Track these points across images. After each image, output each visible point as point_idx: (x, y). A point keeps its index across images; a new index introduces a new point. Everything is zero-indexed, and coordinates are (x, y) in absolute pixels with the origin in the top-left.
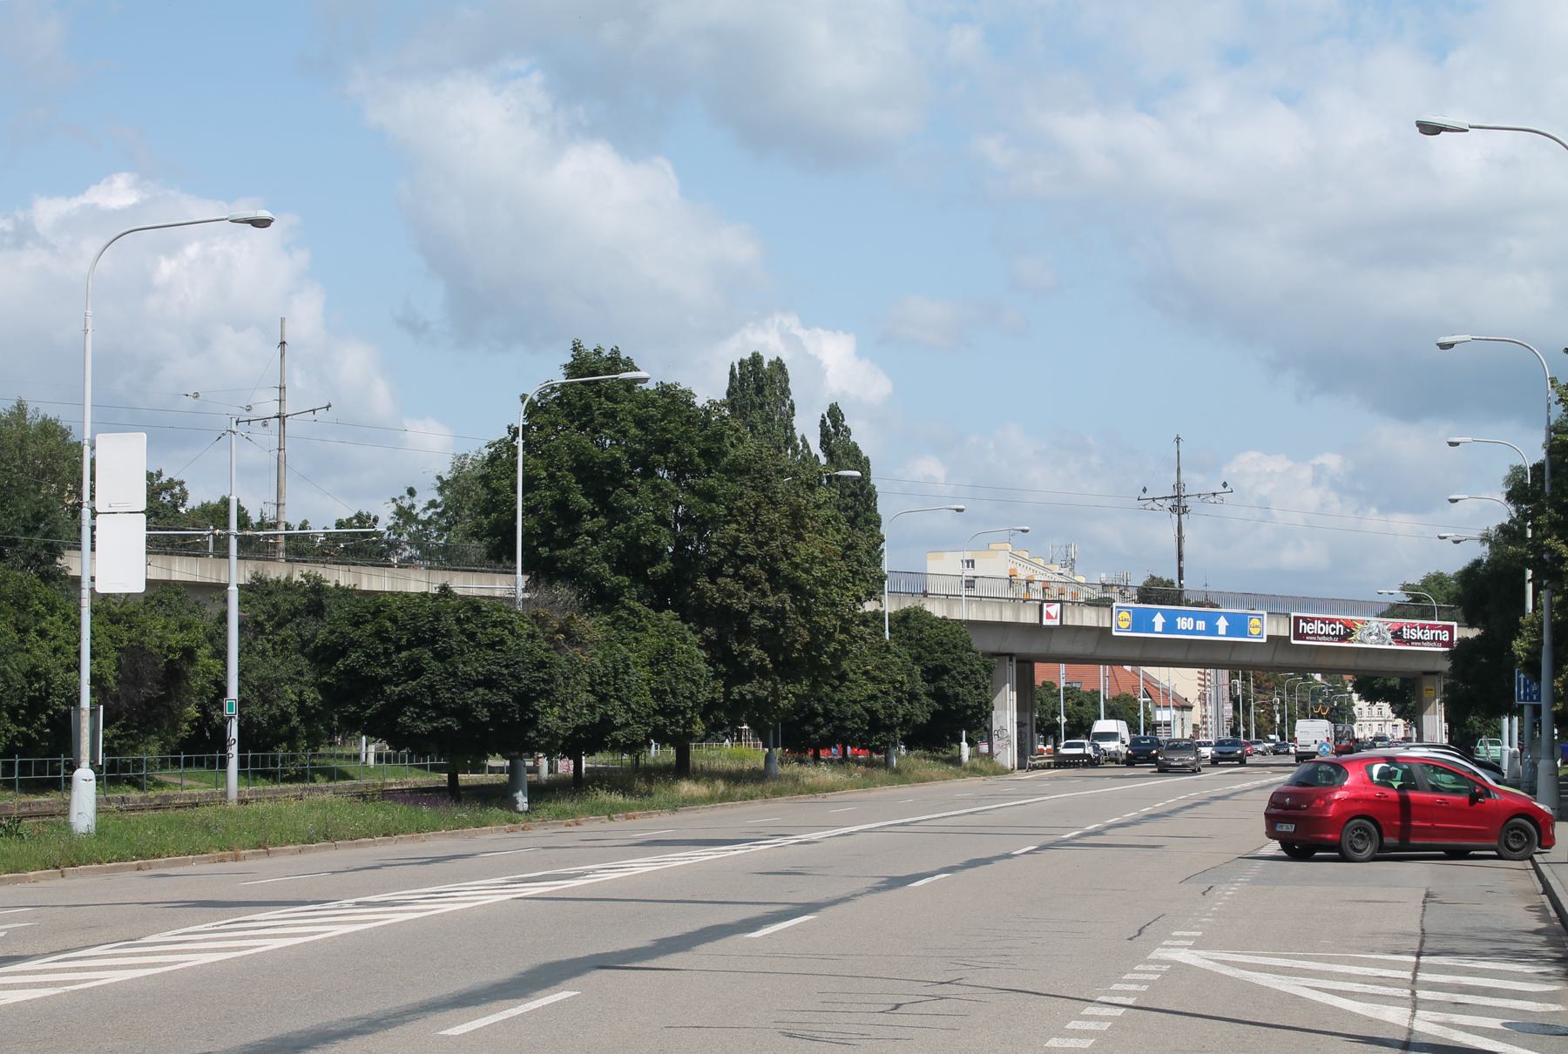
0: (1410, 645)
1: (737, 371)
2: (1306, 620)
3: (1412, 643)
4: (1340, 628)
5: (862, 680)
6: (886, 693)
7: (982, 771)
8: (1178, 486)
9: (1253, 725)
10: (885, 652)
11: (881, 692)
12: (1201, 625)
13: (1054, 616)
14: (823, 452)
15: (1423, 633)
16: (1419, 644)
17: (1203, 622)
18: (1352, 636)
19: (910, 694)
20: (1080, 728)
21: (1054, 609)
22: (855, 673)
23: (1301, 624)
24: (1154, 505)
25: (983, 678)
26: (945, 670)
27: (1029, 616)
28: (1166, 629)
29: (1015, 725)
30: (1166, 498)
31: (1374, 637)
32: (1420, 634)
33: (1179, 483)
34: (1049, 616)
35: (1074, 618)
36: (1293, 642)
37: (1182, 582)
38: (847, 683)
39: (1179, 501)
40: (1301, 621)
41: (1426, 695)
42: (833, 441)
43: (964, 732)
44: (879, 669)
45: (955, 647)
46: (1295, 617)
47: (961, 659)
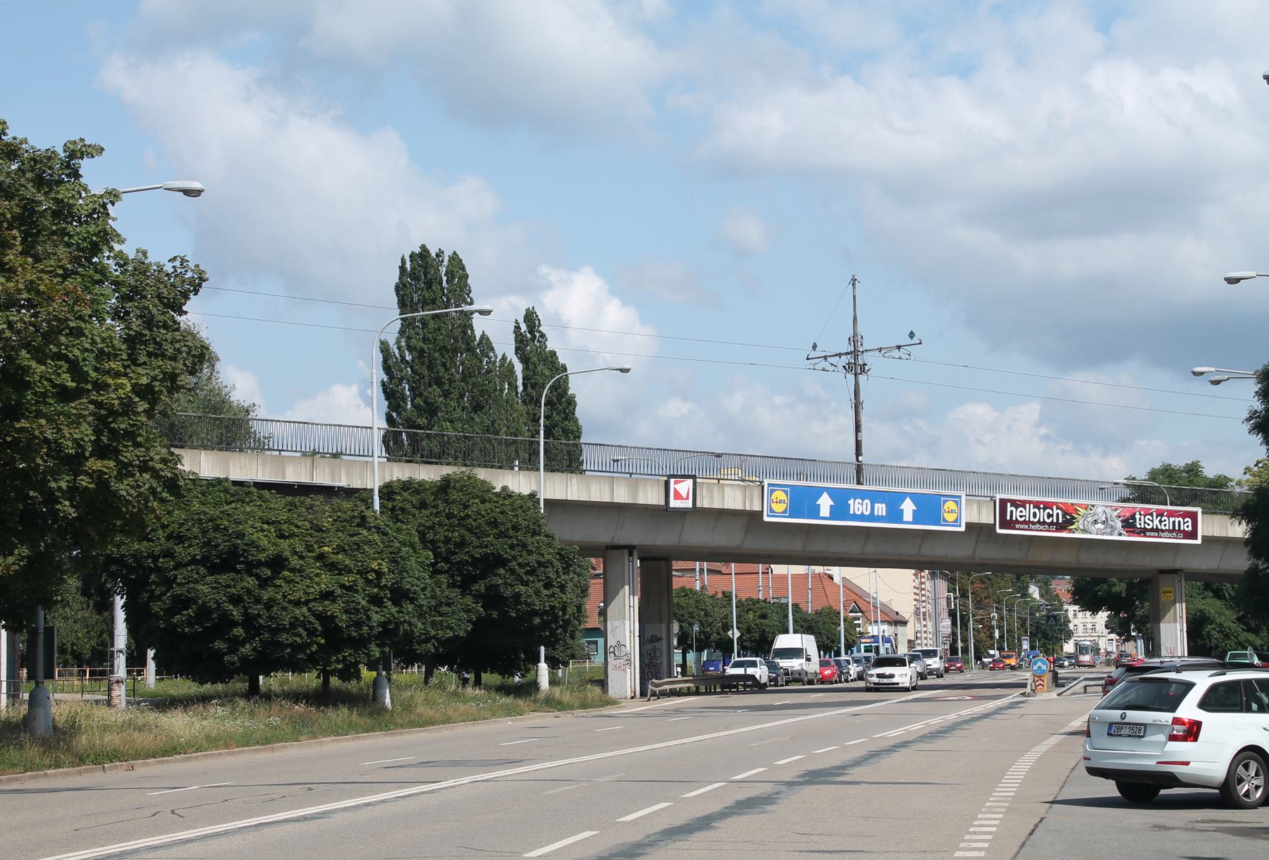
0: (1145, 536)
1: (408, 265)
2: (1015, 504)
3: (1148, 534)
4: (1058, 514)
5: (314, 568)
6: (350, 589)
7: (560, 703)
8: (855, 339)
9: (972, 641)
10: (358, 525)
11: (342, 586)
12: (881, 509)
13: (685, 496)
14: (519, 358)
15: (1161, 522)
16: (1156, 534)
17: (884, 505)
18: (1073, 524)
19: (392, 590)
20: (760, 645)
21: (685, 487)
22: (301, 557)
23: (1009, 508)
24: (824, 364)
25: (557, 572)
26: (500, 561)
27: (651, 496)
28: (834, 514)
29: (637, 639)
30: (840, 355)
31: (1100, 526)
32: (1156, 522)
33: (855, 335)
34: (678, 496)
35: (712, 497)
36: (999, 531)
37: (860, 458)
38: (286, 573)
39: (856, 357)
40: (1009, 504)
41: (1164, 598)
42: (529, 348)
43: (542, 648)
44: (344, 550)
45: (515, 528)
46: (1001, 500)
47: (524, 546)
